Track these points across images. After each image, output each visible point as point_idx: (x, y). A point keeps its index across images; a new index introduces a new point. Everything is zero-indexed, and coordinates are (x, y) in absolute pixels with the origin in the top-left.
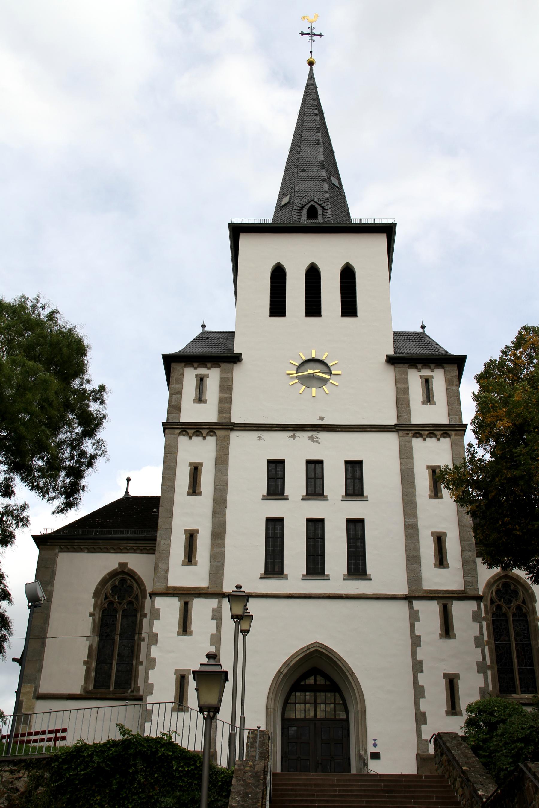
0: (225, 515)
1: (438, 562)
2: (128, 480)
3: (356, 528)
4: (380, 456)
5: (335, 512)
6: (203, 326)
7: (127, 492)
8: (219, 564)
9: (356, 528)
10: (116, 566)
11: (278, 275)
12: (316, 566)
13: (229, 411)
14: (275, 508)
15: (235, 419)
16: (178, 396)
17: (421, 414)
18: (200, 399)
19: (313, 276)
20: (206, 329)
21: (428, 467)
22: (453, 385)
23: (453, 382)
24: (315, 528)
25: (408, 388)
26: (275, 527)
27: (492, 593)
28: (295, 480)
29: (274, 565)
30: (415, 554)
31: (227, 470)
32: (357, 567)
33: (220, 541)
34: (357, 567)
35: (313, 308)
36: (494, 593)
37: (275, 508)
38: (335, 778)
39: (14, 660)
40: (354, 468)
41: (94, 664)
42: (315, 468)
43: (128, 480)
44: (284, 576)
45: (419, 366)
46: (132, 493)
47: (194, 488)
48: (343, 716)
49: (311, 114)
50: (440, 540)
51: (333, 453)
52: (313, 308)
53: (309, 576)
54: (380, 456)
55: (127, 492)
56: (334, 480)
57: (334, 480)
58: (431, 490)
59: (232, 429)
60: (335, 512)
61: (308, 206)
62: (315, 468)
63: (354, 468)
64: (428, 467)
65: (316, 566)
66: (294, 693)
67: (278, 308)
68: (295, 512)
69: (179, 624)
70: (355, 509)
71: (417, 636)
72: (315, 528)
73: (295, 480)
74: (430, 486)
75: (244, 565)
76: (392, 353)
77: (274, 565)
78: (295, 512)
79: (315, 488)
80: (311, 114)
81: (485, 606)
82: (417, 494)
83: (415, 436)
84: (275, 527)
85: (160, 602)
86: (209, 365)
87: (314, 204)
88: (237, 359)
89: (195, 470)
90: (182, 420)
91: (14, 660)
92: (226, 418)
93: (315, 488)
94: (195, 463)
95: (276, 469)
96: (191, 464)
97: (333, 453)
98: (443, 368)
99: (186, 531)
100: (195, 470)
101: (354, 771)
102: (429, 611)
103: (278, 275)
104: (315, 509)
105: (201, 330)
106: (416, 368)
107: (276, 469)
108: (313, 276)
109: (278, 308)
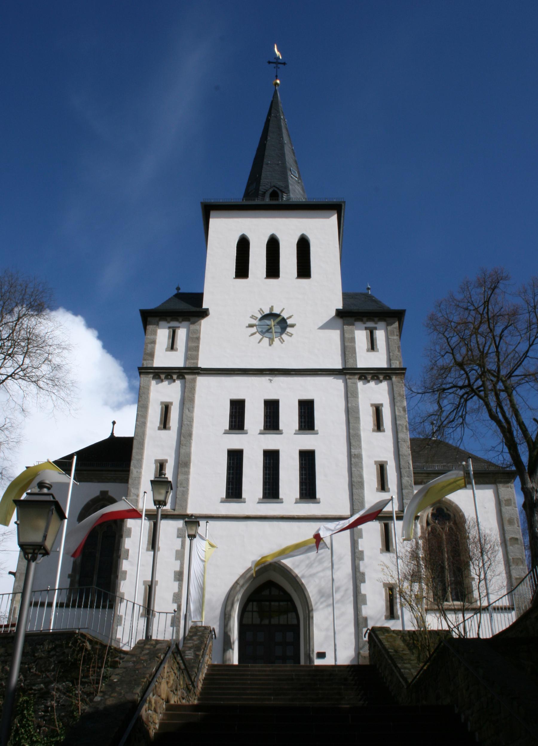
0: (190, 447)
1: (380, 487)
2: (114, 423)
3: (307, 459)
4: (329, 396)
5: (289, 443)
6: (178, 289)
7: (112, 434)
8: (184, 489)
9: (307, 459)
10: (97, 493)
11: (243, 245)
12: (271, 490)
13: (196, 358)
14: (236, 441)
15: (202, 364)
16: (153, 345)
17: (365, 359)
18: (172, 347)
19: (273, 246)
20: (180, 291)
21: (372, 405)
22: (394, 335)
23: (394, 332)
24: (271, 459)
25: (354, 338)
26: (235, 458)
27: (428, 516)
28: (255, 416)
29: (234, 490)
30: (360, 480)
31: (193, 408)
32: (308, 491)
33: (186, 469)
34: (308, 491)
35: (273, 270)
36: (430, 516)
37: (236, 441)
38: (288, 667)
39: (10, 573)
40: (306, 409)
41: (77, 578)
42: (272, 408)
43: (114, 423)
44: (242, 500)
45: (365, 319)
46: (116, 435)
47: (165, 424)
48: (295, 622)
49: (273, 105)
50: (382, 468)
51: (289, 394)
52: (273, 270)
53: (265, 500)
54: (329, 396)
55: (112, 434)
56: (289, 417)
57: (289, 417)
58: (374, 424)
59: (198, 374)
60: (289, 443)
61: (271, 190)
62: (272, 408)
63: (306, 409)
64: (372, 405)
65: (271, 490)
66: (251, 603)
67: (242, 270)
68: (254, 444)
69: (148, 542)
70: (307, 442)
71: (176, 602)
72: (271, 459)
73: (255, 416)
74: (374, 421)
75: (205, 489)
76: (340, 307)
77: (234, 490)
78: (254, 444)
79: (272, 422)
80: (273, 105)
81: (422, 527)
82: (361, 428)
83: (360, 379)
84: (235, 458)
85: (130, 523)
86: (180, 319)
87: (276, 189)
88: (205, 313)
89: (166, 409)
90: (155, 365)
91: (10, 573)
92: (194, 363)
93: (272, 422)
94: (165, 402)
95: (237, 408)
96: (162, 403)
97: (289, 394)
98: (385, 320)
99: (156, 461)
100: (166, 409)
101: (302, 662)
102: (372, 530)
103: (243, 245)
104: (271, 442)
105: (175, 292)
106: (362, 320)
107: (237, 408)
108: (273, 246)
109: (242, 270)
